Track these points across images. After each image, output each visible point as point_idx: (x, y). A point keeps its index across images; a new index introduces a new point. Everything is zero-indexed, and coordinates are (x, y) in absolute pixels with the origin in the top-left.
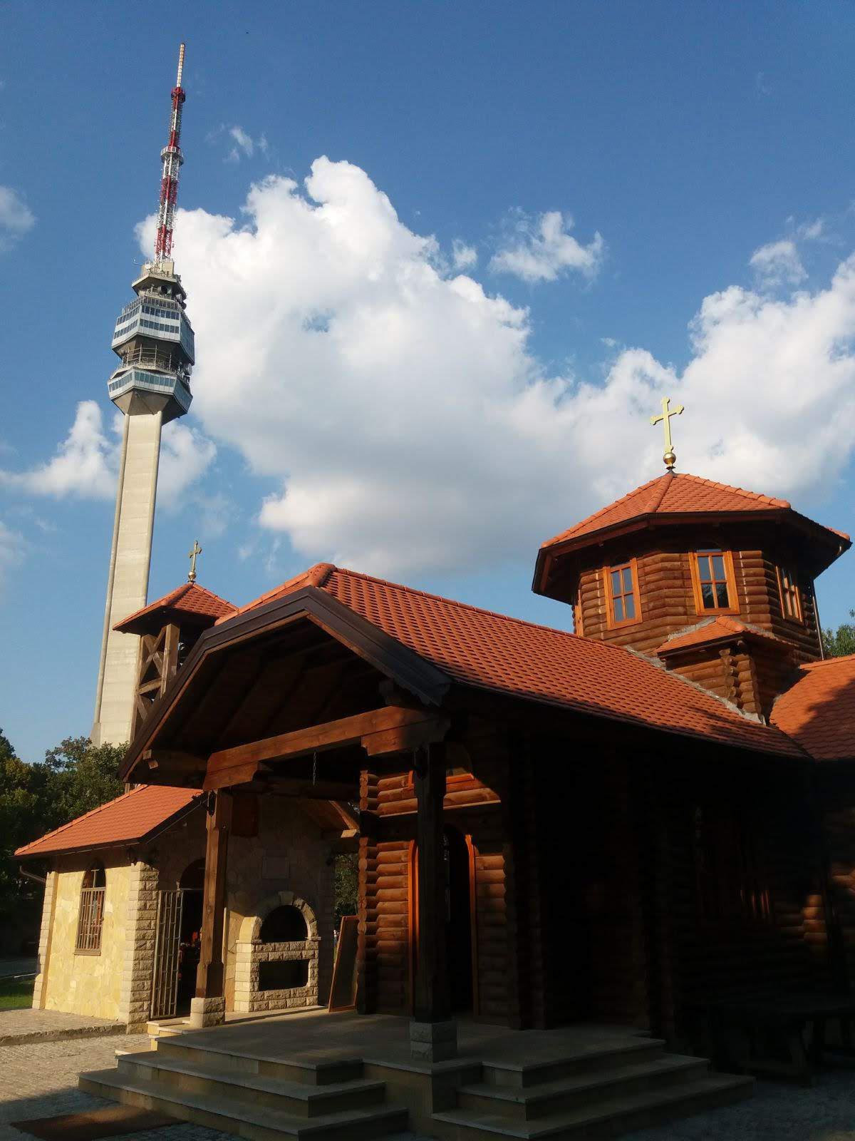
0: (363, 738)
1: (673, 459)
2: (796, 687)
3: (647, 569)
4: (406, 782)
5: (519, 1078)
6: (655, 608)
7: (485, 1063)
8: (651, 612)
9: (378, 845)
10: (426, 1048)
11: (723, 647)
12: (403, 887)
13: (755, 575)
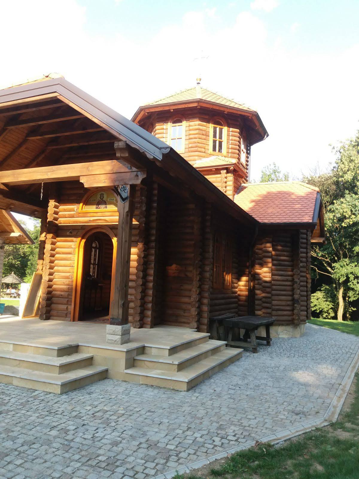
0: (81, 178)
1: (200, 80)
2: (242, 192)
3: (191, 128)
4: (78, 208)
5: (167, 352)
6: (192, 147)
7: (146, 345)
8: (190, 149)
9: (57, 238)
10: (118, 338)
11: (223, 169)
12: (71, 260)
13: (235, 140)
